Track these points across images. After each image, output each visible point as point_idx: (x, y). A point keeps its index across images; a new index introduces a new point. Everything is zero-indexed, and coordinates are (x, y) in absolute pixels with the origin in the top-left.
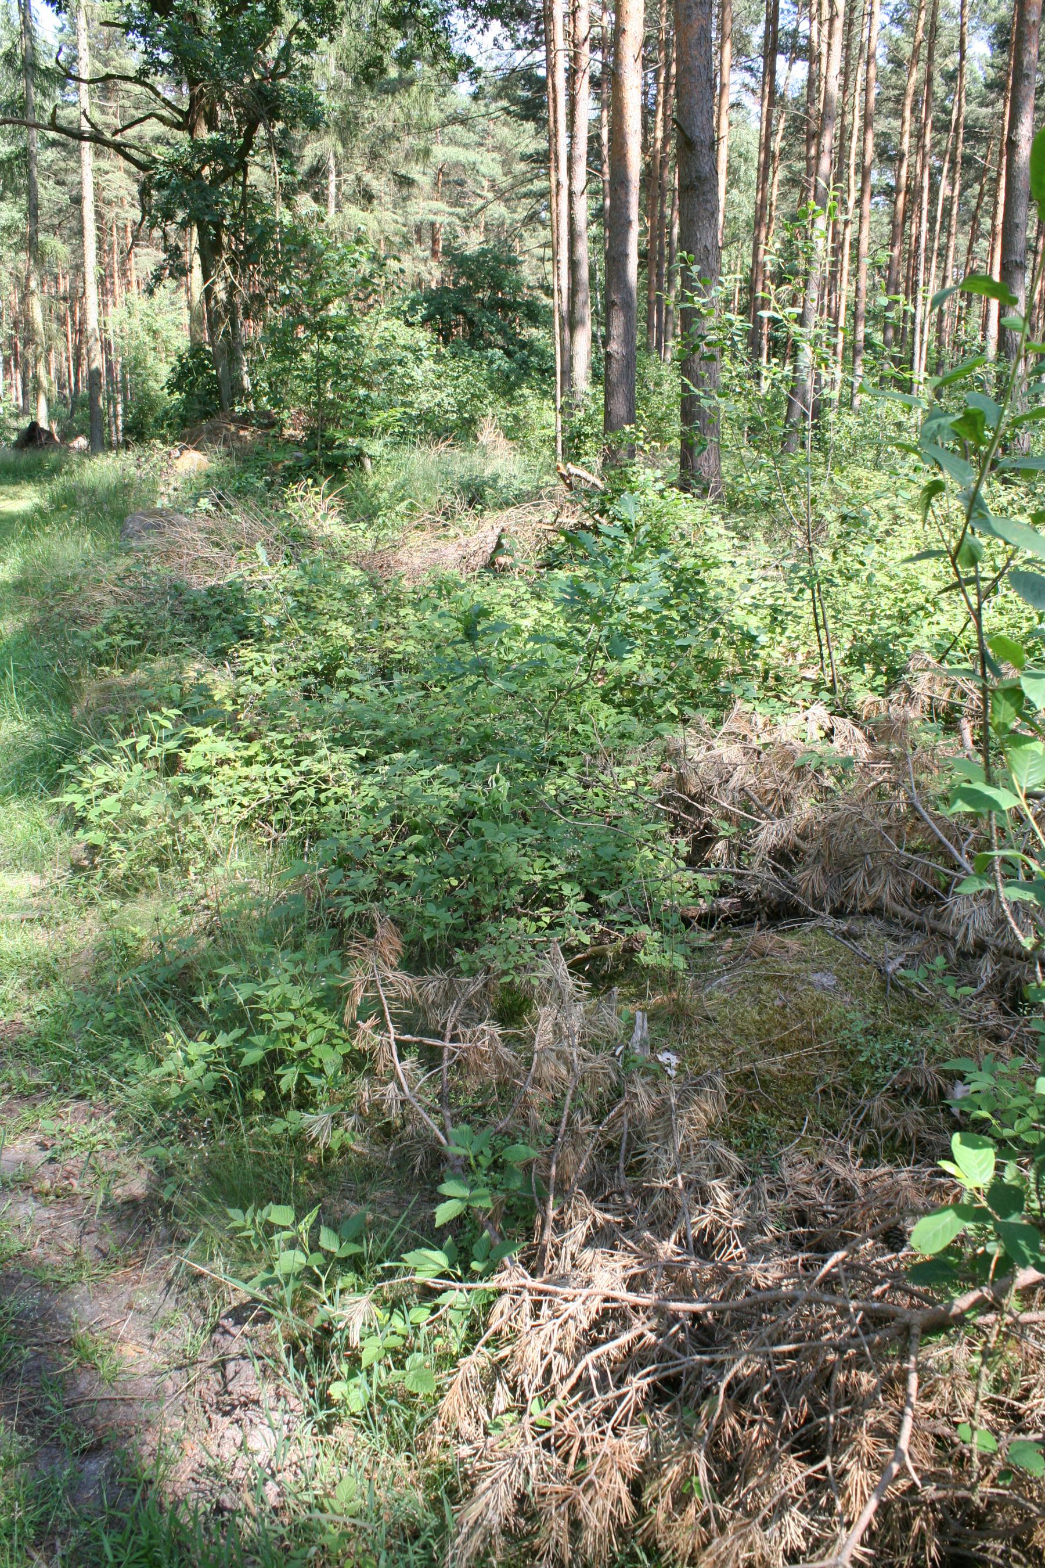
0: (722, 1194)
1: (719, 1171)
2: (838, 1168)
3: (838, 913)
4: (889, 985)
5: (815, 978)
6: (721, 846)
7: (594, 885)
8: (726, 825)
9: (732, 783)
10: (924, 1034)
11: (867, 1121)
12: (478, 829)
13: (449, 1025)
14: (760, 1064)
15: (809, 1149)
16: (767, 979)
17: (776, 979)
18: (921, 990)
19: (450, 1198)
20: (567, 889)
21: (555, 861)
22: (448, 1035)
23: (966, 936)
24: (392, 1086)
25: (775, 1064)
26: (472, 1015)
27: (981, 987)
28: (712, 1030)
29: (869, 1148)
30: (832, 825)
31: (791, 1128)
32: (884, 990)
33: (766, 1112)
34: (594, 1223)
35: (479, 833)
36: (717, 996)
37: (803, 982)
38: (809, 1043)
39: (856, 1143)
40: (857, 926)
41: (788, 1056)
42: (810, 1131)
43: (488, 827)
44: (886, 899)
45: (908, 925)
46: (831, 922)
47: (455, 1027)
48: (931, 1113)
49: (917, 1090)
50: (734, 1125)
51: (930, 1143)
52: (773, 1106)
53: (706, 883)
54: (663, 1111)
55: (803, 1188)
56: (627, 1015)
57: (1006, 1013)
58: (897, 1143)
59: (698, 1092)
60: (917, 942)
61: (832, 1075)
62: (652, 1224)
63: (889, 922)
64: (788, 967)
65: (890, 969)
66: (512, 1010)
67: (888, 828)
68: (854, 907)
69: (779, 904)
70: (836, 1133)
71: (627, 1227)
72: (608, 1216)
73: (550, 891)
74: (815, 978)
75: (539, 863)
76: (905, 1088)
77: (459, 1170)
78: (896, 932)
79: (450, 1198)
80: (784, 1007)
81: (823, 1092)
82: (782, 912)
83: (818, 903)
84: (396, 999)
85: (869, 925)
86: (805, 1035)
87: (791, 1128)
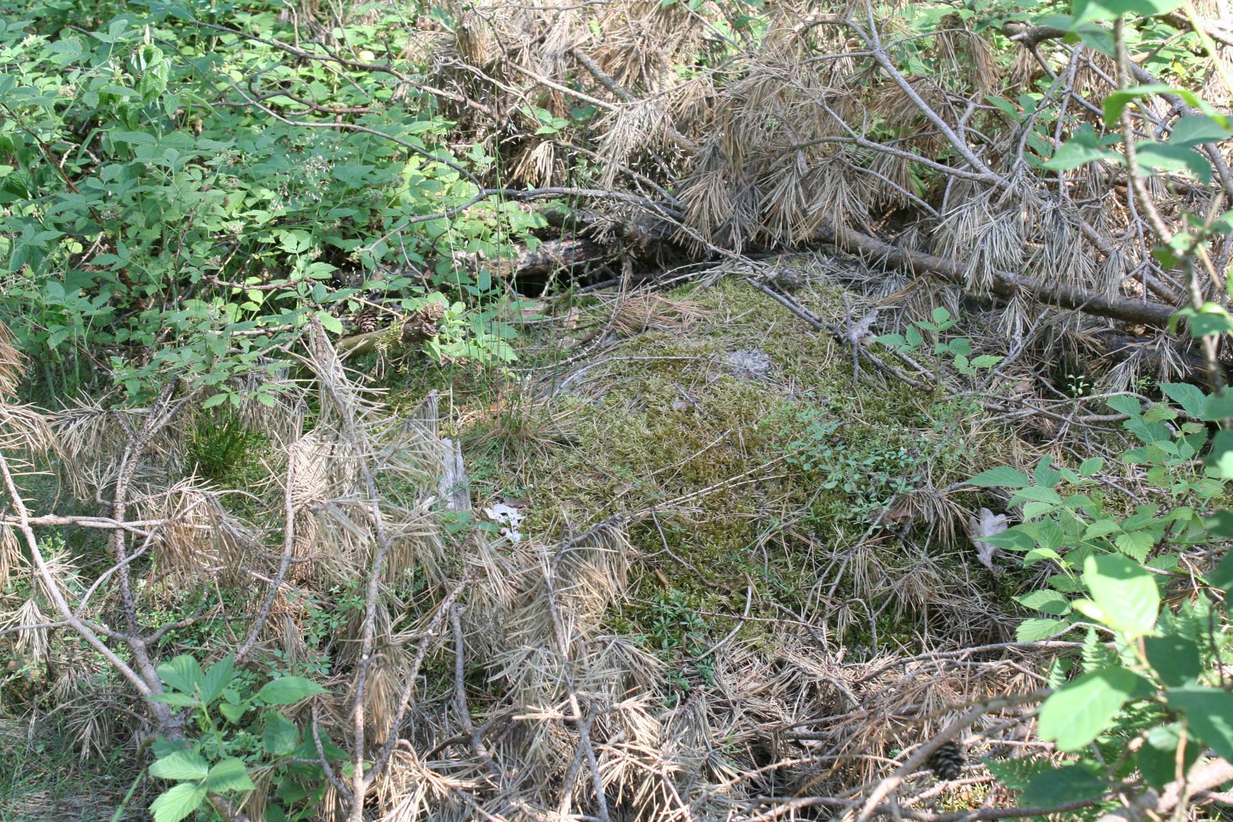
0: (640, 721)
1: (630, 685)
2: (805, 663)
3: (756, 250)
4: (856, 363)
5: (732, 360)
6: (541, 154)
7: (333, 233)
8: (546, 115)
9: (550, 46)
10: (926, 436)
11: (847, 586)
12: (121, 146)
13: (120, 491)
14: (662, 508)
15: (758, 640)
16: (653, 367)
17: (670, 366)
18: (908, 366)
19: (174, 783)
20: (291, 242)
21: (267, 194)
22: (121, 508)
23: (980, 268)
24: (29, 608)
25: (683, 508)
26: (154, 473)
27: (1013, 354)
28: (572, 459)
29: (853, 629)
30: (739, 101)
31: (725, 608)
32: (849, 371)
33: (681, 586)
34: (429, 794)
35: (124, 152)
36: (571, 403)
37: (714, 368)
38: (738, 466)
39: (833, 623)
40: (793, 271)
41: (704, 491)
42: (755, 610)
43: (137, 138)
44: (838, 223)
45: (873, 262)
46: (748, 267)
47: (128, 497)
48: (945, 566)
49: (920, 529)
50: (629, 612)
51: (950, 612)
52: (691, 575)
53: (522, 217)
54: (530, 593)
55: (757, 705)
56: (438, 448)
57: (1048, 394)
58: (898, 618)
59: (585, 556)
60: (893, 290)
61: (783, 519)
62: (525, 786)
63: (843, 263)
64: (686, 345)
65: (854, 336)
66: (221, 453)
67: (832, 101)
68: (784, 239)
69: (652, 243)
70: (797, 609)
71: (485, 794)
72: (452, 781)
73: (257, 247)
74: (732, 360)
75: (236, 198)
76: (900, 529)
77: (176, 736)
78: (856, 276)
79: (174, 783)
80: (690, 411)
81: (770, 544)
82: (664, 256)
83: (721, 234)
84: (19, 453)
85: (811, 266)
86: (729, 454)
87: (725, 608)
